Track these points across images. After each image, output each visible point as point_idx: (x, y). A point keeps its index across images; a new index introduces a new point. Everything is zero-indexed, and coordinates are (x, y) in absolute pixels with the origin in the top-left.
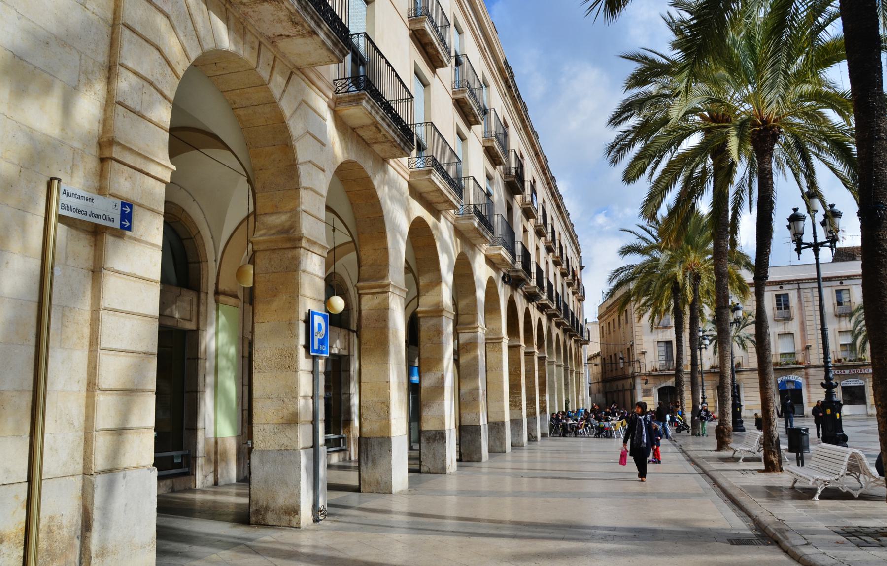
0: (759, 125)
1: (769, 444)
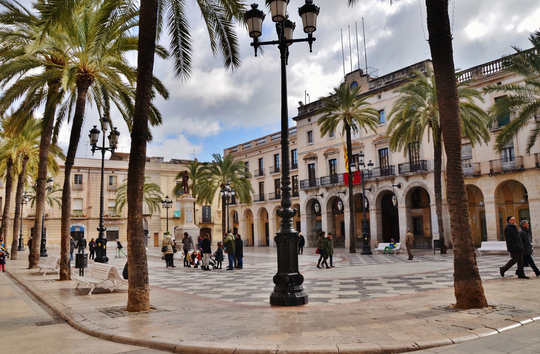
0: (82, 73)
1: (64, 263)
